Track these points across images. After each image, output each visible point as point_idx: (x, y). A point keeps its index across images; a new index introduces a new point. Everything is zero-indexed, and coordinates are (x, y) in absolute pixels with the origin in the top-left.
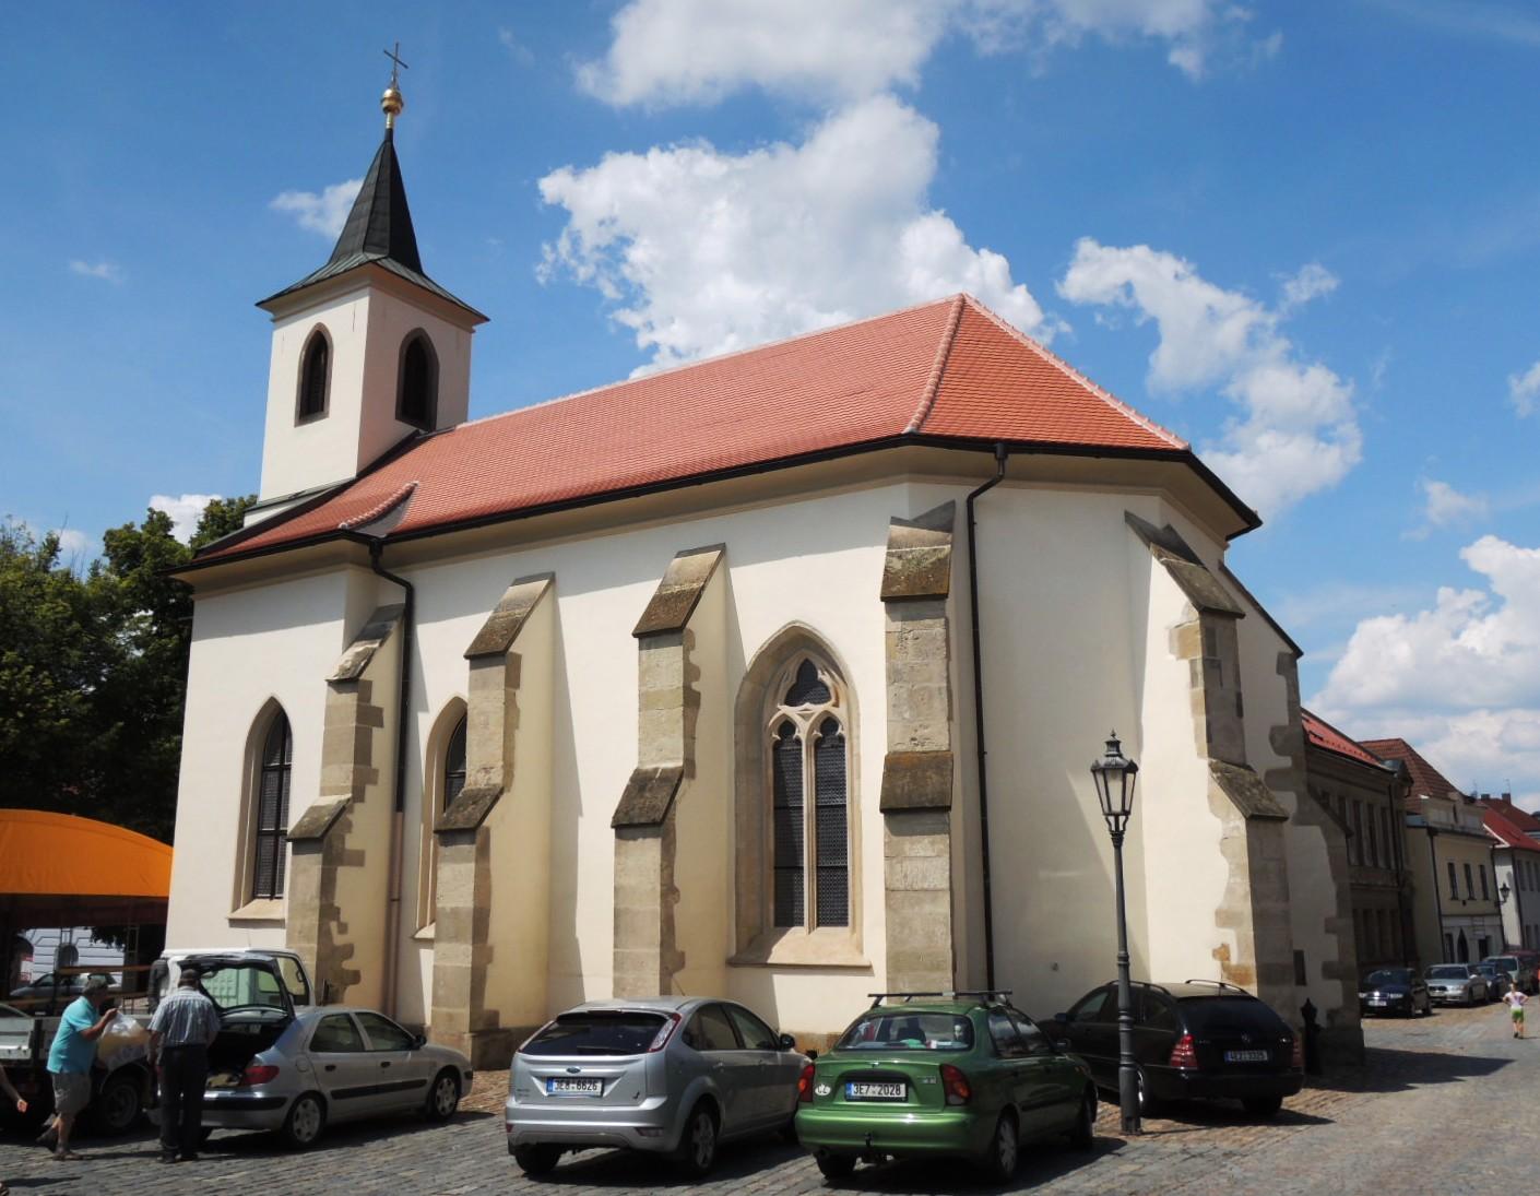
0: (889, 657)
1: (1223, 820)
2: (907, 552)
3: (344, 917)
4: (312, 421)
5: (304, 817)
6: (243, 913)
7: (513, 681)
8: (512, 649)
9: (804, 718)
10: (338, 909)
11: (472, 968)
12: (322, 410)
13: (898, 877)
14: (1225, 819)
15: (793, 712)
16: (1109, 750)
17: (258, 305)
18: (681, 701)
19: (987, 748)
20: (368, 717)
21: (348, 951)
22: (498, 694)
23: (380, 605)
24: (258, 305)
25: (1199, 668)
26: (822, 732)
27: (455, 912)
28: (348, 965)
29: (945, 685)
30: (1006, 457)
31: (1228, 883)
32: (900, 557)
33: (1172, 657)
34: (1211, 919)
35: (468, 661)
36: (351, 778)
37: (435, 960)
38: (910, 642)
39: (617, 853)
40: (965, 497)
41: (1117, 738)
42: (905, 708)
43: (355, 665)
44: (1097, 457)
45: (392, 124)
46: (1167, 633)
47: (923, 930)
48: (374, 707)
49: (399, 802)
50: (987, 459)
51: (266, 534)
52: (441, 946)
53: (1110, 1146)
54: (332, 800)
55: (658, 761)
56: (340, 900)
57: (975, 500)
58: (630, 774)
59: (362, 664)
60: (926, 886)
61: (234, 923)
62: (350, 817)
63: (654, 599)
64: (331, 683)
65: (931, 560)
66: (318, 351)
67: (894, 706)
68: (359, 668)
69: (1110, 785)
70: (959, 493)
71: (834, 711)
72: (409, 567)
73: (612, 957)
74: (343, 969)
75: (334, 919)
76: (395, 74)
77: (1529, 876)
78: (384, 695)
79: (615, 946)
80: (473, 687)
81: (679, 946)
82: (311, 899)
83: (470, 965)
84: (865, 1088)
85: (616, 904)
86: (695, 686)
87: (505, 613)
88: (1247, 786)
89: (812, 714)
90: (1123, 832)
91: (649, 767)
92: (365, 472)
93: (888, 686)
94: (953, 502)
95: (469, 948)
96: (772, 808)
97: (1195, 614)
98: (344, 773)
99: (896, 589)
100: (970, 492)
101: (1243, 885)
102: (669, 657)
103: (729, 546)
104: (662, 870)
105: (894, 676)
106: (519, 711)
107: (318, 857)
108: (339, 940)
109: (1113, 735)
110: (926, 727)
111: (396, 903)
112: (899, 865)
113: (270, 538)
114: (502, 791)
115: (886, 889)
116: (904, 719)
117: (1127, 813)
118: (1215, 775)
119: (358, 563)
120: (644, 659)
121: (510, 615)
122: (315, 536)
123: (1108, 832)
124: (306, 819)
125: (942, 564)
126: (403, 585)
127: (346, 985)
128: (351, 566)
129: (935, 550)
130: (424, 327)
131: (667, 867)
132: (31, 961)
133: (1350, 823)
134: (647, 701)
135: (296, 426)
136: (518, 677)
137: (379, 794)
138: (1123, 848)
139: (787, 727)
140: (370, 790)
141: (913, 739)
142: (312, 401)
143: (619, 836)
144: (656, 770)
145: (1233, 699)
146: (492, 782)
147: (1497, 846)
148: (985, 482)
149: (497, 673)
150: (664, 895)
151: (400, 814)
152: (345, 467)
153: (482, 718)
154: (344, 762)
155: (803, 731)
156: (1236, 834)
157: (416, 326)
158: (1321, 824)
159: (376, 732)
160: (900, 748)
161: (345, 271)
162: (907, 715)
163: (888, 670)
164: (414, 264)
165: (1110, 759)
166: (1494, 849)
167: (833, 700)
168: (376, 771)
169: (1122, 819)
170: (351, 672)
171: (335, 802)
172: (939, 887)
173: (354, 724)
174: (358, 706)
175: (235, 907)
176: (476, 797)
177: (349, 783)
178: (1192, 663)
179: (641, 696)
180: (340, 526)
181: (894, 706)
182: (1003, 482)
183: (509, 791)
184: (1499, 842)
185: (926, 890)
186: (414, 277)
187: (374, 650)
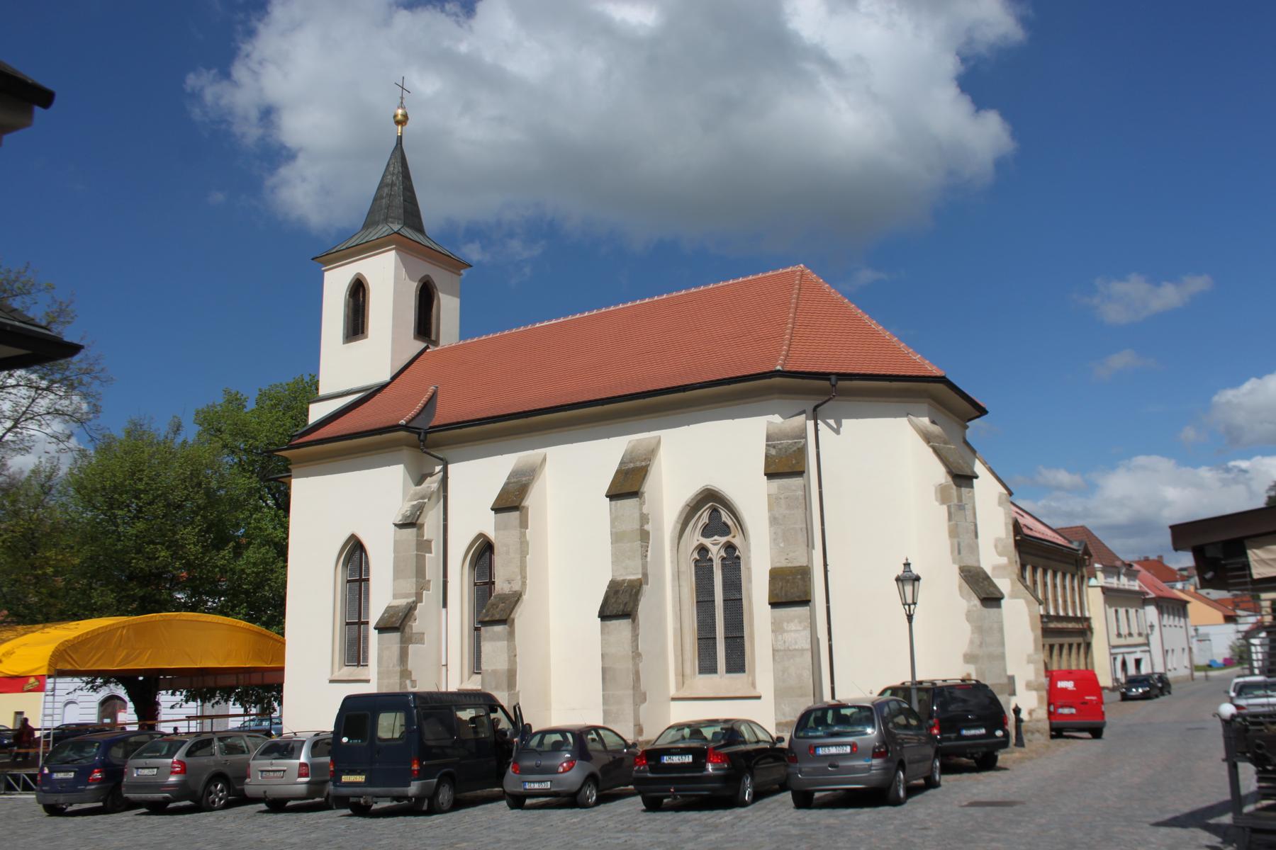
0: (770, 509)
6: (337, 676)
7: (524, 524)
12: (363, 332)
13: (779, 643)
14: (969, 601)
15: (707, 542)
27: (495, 672)
29: (804, 526)
32: (774, 447)
33: (937, 504)
34: (961, 660)
36: (414, 587)
39: (602, 633)
40: (812, 407)
41: (909, 561)
43: (412, 514)
45: (401, 133)
50: (825, 384)
53: (744, 804)
54: (402, 602)
56: (411, 664)
57: (819, 409)
58: (607, 583)
59: (418, 513)
61: (332, 681)
63: (617, 472)
64: (396, 525)
66: (358, 290)
67: (774, 540)
68: (417, 516)
69: (905, 588)
72: (443, 448)
76: (402, 98)
79: (603, 690)
80: (497, 528)
81: (643, 688)
82: (393, 666)
84: (684, 757)
86: (646, 527)
87: (515, 480)
88: (981, 580)
91: (620, 578)
92: (394, 378)
96: (695, 601)
98: (409, 585)
105: (774, 521)
109: (907, 560)
110: (794, 552)
112: (781, 636)
115: (773, 650)
117: (915, 603)
120: (613, 511)
121: (519, 481)
123: (905, 615)
124: (386, 615)
128: (405, 447)
129: (796, 442)
130: (431, 275)
132: (125, 712)
133: (1040, 596)
134: (617, 538)
135: (344, 343)
136: (527, 522)
138: (913, 624)
139: (703, 550)
141: (787, 559)
142: (356, 326)
143: (602, 620)
144: (624, 581)
145: (973, 527)
146: (514, 590)
147: (1147, 597)
148: (826, 398)
150: (634, 658)
153: (505, 549)
155: (716, 552)
157: (425, 274)
158: (1025, 598)
160: (778, 565)
163: (770, 518)
167: (732, 535)
169: (912, 607)
170: (411, 519)
171: (405, 604)
172: (804, 648)
176: (503, 598)
177: (414, 591)
182: (836, 398)
184: (1148, 594)
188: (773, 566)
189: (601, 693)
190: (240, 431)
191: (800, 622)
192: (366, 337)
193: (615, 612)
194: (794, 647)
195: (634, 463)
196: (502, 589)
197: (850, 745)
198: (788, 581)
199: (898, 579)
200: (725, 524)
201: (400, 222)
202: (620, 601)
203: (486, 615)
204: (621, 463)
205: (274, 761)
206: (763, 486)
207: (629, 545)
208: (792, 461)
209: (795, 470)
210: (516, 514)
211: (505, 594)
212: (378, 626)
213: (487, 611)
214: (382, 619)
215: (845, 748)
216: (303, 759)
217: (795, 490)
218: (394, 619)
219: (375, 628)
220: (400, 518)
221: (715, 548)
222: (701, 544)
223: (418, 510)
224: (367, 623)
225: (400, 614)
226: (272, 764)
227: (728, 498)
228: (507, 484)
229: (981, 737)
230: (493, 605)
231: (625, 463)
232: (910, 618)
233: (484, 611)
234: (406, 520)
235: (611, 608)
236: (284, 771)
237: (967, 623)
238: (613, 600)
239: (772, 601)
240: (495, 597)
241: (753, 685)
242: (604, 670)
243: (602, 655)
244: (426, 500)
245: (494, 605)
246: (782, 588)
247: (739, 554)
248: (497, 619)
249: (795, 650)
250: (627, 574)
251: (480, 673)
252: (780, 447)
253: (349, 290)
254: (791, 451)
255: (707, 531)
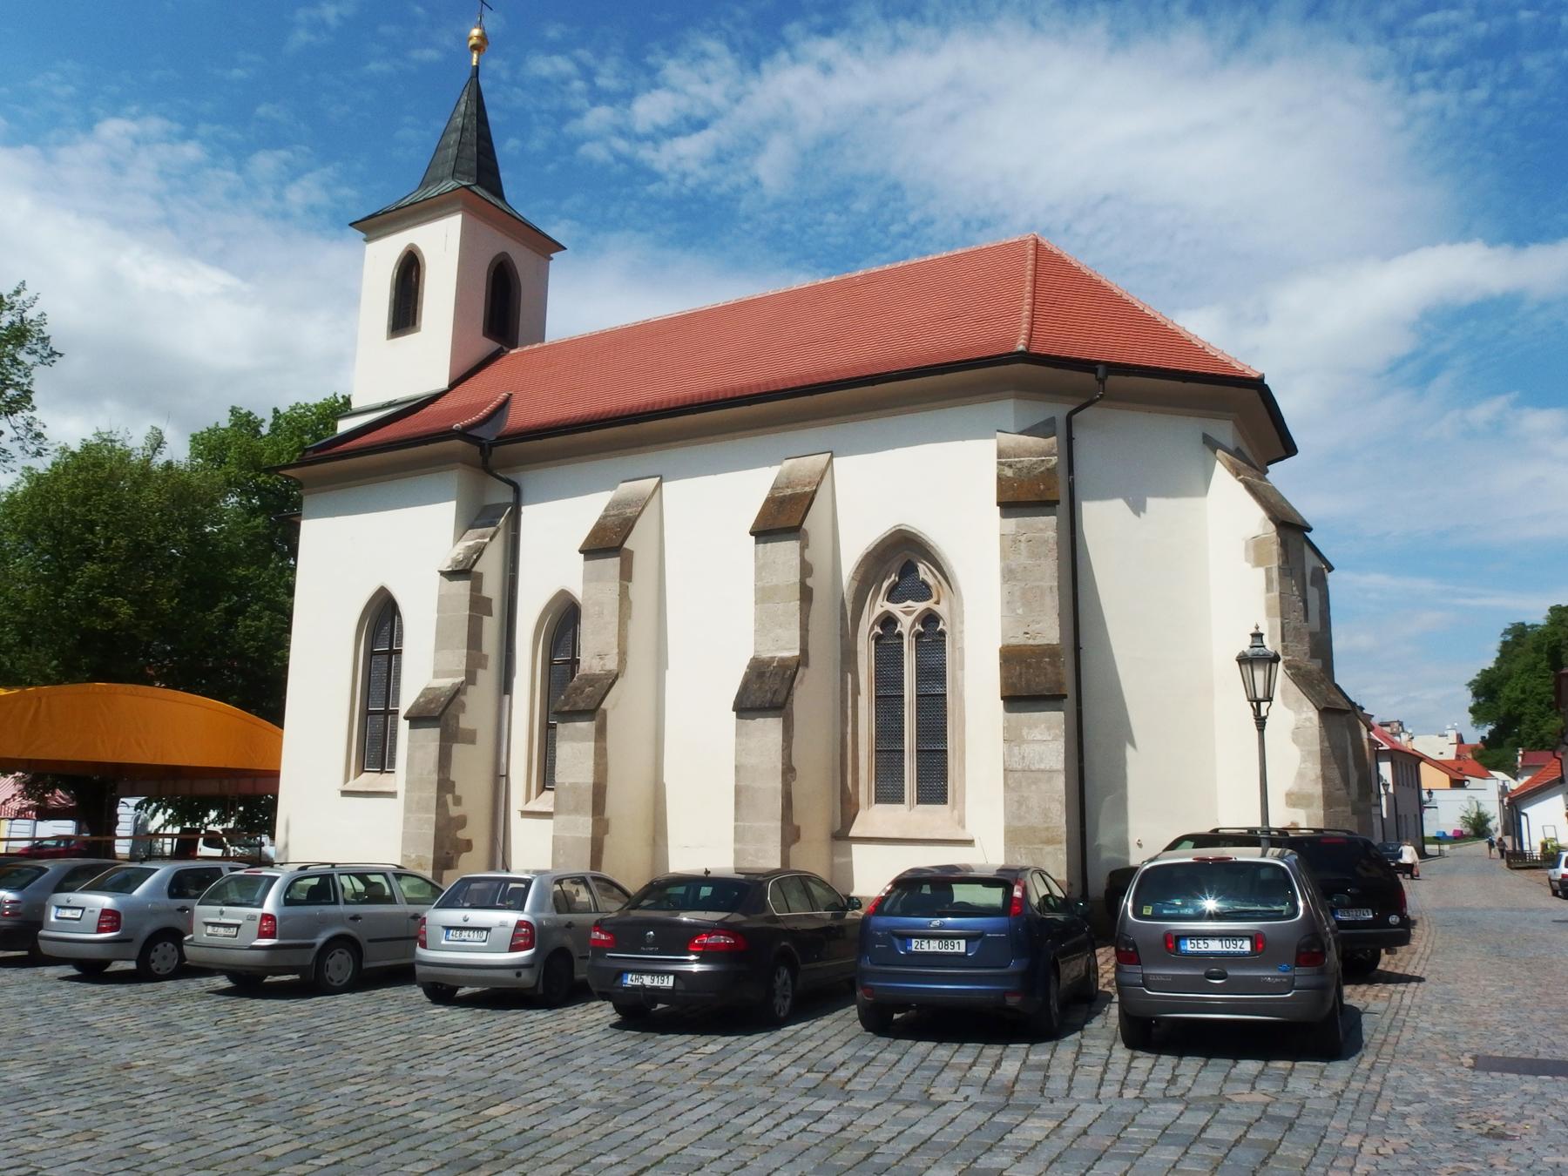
0: (1004, 556)
1: (1295, 712)
2: (1016, 462)
3: (458, 792)
4: (404, 334)
5: (420, 697)
7: (626, 574)
8: (625, 546)
9: (907, 615)
10: (453, 783)
11: (592, 838)
12: (414, 323)
14: (1298, 711)
15: (896, 609)
16: (1253, 642)
17: (351, 225)
18: (798, 596)
19: (1083, 643)
20: (479, 605)
21: (462, 822)
22: (614, 586)
23: (487, 504)
24: (351, 225)
25: (1275, 574)
26: (923, 627)
27: (575, 787)
28: (462, 834)
30: (1107, 377)
31: (1300, 768)
32: (1010, 466)
33: (1248, 566)
35: (754, 537)
37: (554, 830)
38: (1023, 545)
41: (1261, 630)
42: (1019, 604)
43: (467, 558)
44: (1184, 382)
45: (478, 62)
46: (1244, 543)
47: (1039, 807)
48: (484, 597)
49: (506, 686)
50: (1087, 378)
51: (366, 437)
52: (559, 818)
54: (447, 683)
55: (776, 650)
56: (455, 774)
59: (475, 557)
60: (1042, 766)
61: (345, 793)
62: (463, 698)
63: (767, 501)
64: (443, 573)
65: (1041, 470)
66: (410, 270)
67: (1008, 603)
68: (472, 561)
69: (1255, 673)
70: (1059, 411)
71: (936, 608)
73: (733, 830)
74: (457, 839)
75: (449, 793)
77: (1402, 772)
78: (492, 588)
79: (736, 820)
80: (588, 578)
81: (796, 822)
83: (590, 836)
85: (737, 781)
86: (809, 582)
87: (615, 512)
89: (915, 611)
90: (1265, 718)
91: (766, 655)
92: (454, 385)
93: (1002, 584)
94: (1054, 418)
95: (590, 820)
97: (1272, 527)
98: (457, 658)
99: (1009, 497)
100: (1070, 410)
101: (1314, 769)
102: (786, 551)
103: (664, 476)
104: (783, 750)
105: (1008, 574)
106: (631, 602)
107: (437, 731)
108: (454, 811)
109: (1257, 628)
111: (504, 778)
113: (385, 436)
114: (617, 677)
115: (1005, 770)
116: (1018, 614)
117: (1270, 699)
118: (1288, 672)
119: (466, 462)
120: (760, 555)
121: (621, 514)
122: (427, 436)
124: (421, 700)
125: (1051, 472)
126: (511, 485)
127: (459, 853)
128: (459, 464)
129: (1043, 461)
131: (786, 748)
134: (764, 595)
135: (388, 339)
137: (488, 678)
139: (888, 621)
140: (481, 673)
142: (404, 315)
143: (738, 717)
144: (773, 658)
146: (607, 668)
147: (1380, 748)
148: (1084, 401)
149: (613, 564)
150: (784, 773)
151: (507, 697)
152: (439, 380)
153: (597, 608)
154: (458, 648)
155: (906, 625)
156: (1308, 724)
159: (487, 620)
160: (1014, 641)
161: (439, 195)
162: (1020, 611)
164: (500, 195)
165: (1257, 649)
166: (1378, 750)
167: (935, 599)
168: (486, 657)
169: (1264, 706)
171: (450, 685)
172: (1055, 768)
173: (468, 612)
174: (471, 595)
175: (347, 780)
176: (592, 680)
177: (463, 667)
178: (1268, 571)
179: (757, 590)
180: (454, 427)
181: (1008, 603)
183: (623, 676)
184: (1382, 746)
185: (1043, 771)
186: (499, 203)
187: (486, 544)
188: (1006, 643)
189: (732, 823)
190: (254, 463)
191: (1049, 728)
192: (418, 330)
193: (758, 703)
194: (1037, 766)
195: (793, 488)
196: (590, 667)
197: (1250, 938)
198: (1029, 666)
199: (1243, 660)
200: (924, 583)
201: (471, 179)
202: (767, 688)
203: (566, 703)
204: (773, 488)
205: (224, 908)
206: (990, 521)
207: (781, 606)
208: (1039, 485)
209: (1044, 499)
210: (616, 561)
211: (594, 674)
212: (409, 715)
213: (567, 698)
214: (416, 705)
215: (1239, 943)
216: (270, 905)
217: (1041, 530)
218: (433, 706)
219: (406, 718)
220: (449, 562)
221: (907, 615)
222: (887, 612)
223: (475, 553)
224: (396, 712)
225: (442, 699)
226: (222, 913)
227: (932, 543)
228: (604, 517)
229: (1366, 924)
230: (576, 689)
231: (778, 488)
232: (1261, 722)
233: (563, 697)
234: (456, 566)
235: (752, 697)
236: (238, 926)
237: (1295, 746)
238: (755, 687)
239: (1007, 694)
240: (580, 679)
241: (961, 823)
242: (738, 791)
243: (736, 767)
244: (487, 540)
245: (579, 690)
246: (1021, 674)
247: (944, 628)
248: (581, 709)
249: (1039, 771)
250: (777, 650)
251: (552, 789)
252: (1019, 466)
253: (398, 266)
254: (1037, 471)
255: (894, 595)
